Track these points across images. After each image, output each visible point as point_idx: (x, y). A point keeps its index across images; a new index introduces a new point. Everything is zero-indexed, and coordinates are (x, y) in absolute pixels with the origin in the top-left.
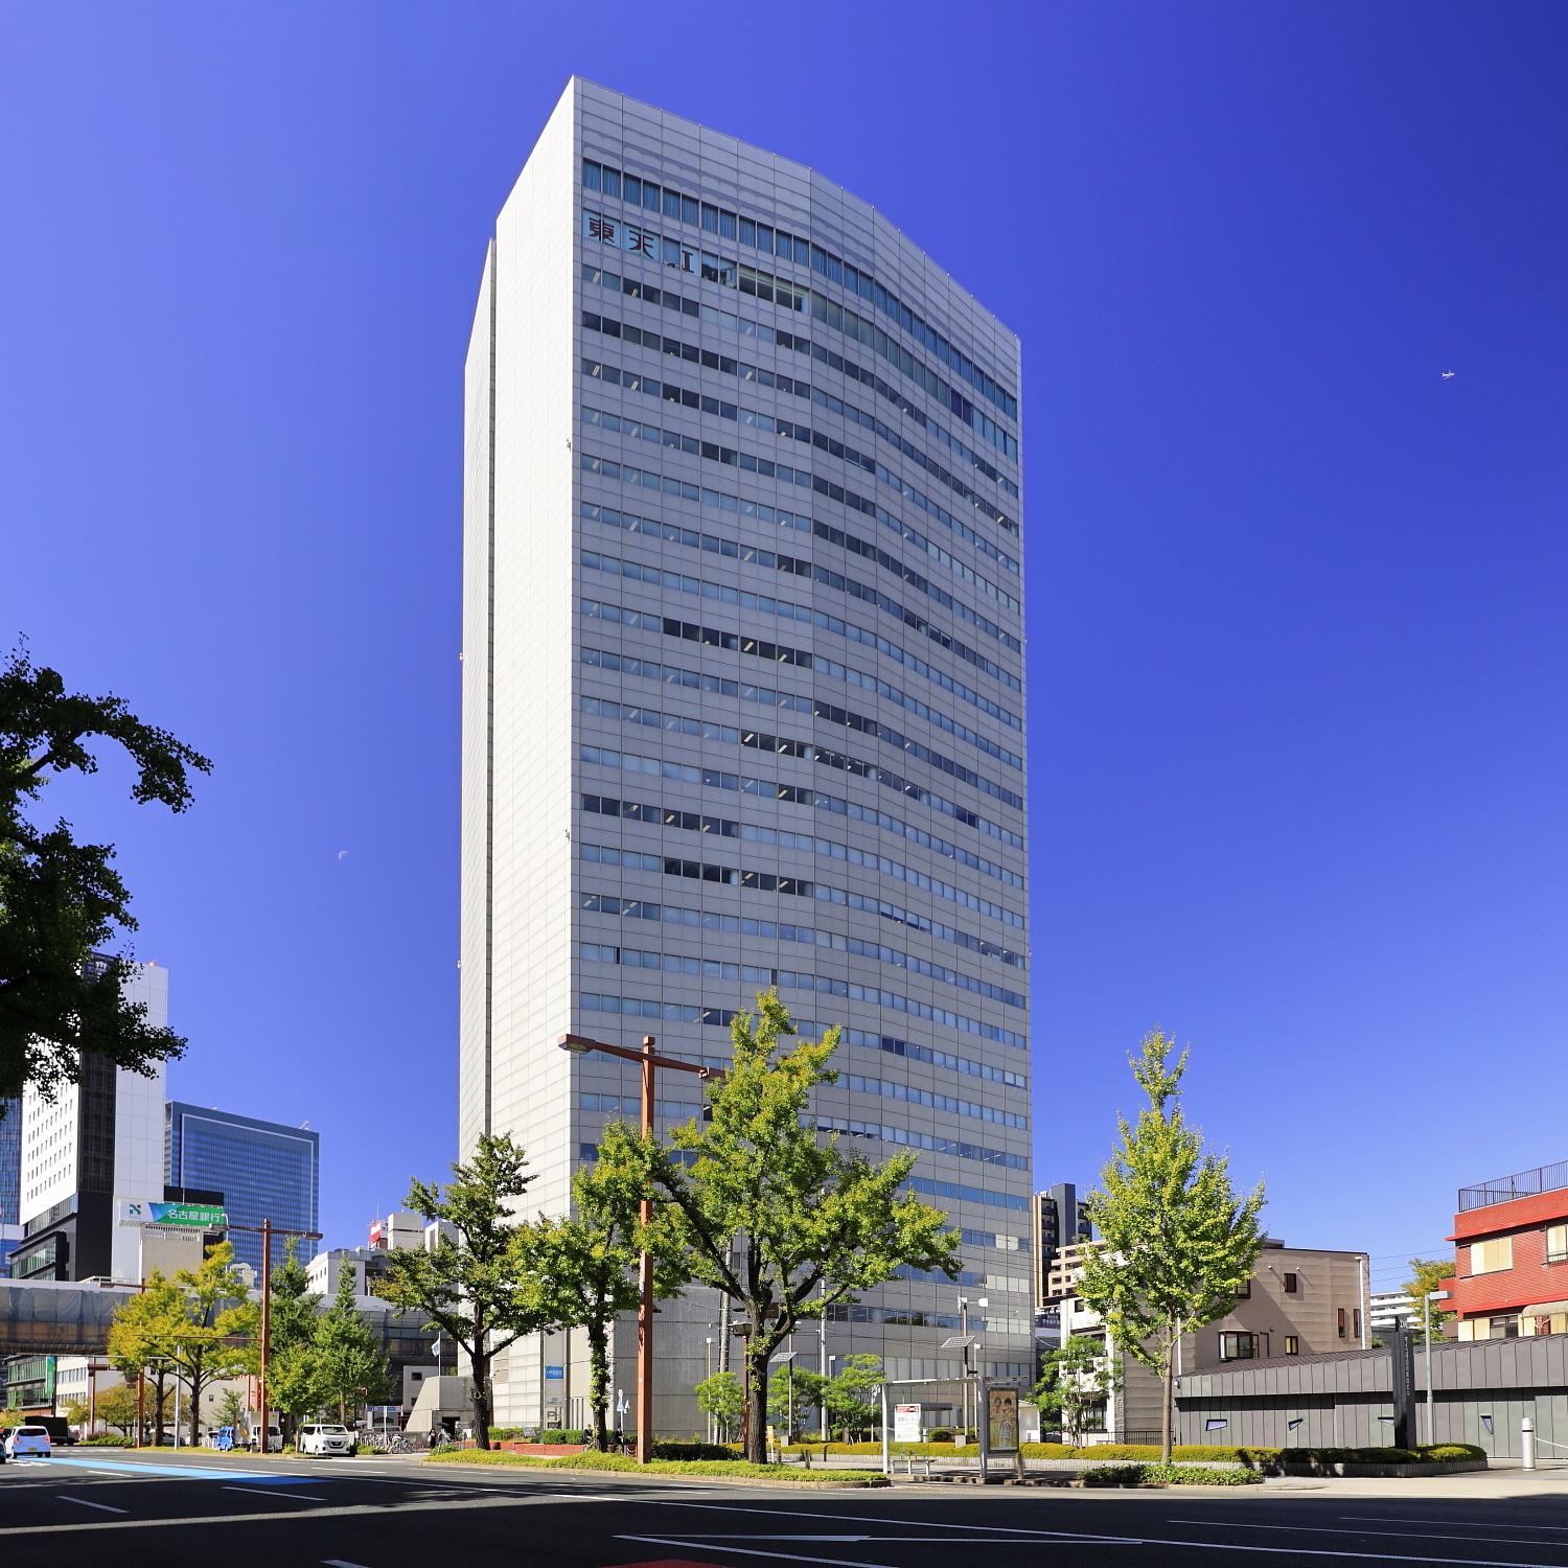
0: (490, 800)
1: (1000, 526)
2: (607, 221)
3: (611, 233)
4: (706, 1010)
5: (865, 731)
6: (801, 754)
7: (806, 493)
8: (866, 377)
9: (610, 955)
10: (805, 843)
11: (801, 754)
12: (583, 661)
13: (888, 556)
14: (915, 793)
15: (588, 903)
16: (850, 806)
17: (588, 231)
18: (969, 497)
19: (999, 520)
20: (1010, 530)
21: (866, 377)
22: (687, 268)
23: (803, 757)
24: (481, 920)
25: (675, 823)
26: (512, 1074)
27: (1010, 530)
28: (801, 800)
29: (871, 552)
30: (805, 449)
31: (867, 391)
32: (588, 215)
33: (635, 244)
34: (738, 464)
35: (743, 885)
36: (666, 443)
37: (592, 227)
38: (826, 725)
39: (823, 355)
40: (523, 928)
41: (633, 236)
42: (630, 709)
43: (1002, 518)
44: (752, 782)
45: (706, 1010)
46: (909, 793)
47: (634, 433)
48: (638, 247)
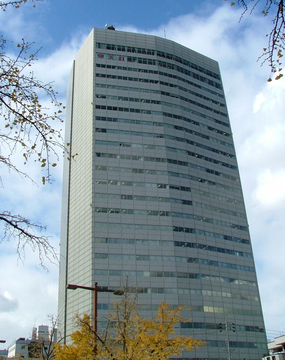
0: (72, 107)
1: (220, 106)
2: (102, 54)
3: (103, 56)
4: (137, 255)
5: (191, 233)
6: (165, 187)
7: (166, 164)
8: (175, 77)
9: (104, 240)
10: (173, 259)
11: (165, 187)
12: (96, 143)
13: (186, 118)
14: (207, 220)
15: (98, 210)
16: (179, 174)
17: (97, 56)
18: (214, 130)
19: (219, 105)
20: (228, 136)
21: (175, 77)
22: (123, 60)
23: (166, 188)
24: (66, 231)
25: (125, 198)
26: (73, 280)
27: (228, 136)
28: (167, 215)
29: (195, 246)
30: (157, 75)
31: (176, 80)
32: (97, 54)
33: (110, 58)
34: (140, 99)
35: (148, 215)
36: (119, 99)
37: (98, 55)
38: (173, 178)
39: (161, 73)
40: (78, 253)
41: (109, 56)
42: (109, 96)
43: (220, 104)
44: (148, 170)
45: (137, 255)
46: (200, 181)
47: (110, 98)
48: (111, 58)
